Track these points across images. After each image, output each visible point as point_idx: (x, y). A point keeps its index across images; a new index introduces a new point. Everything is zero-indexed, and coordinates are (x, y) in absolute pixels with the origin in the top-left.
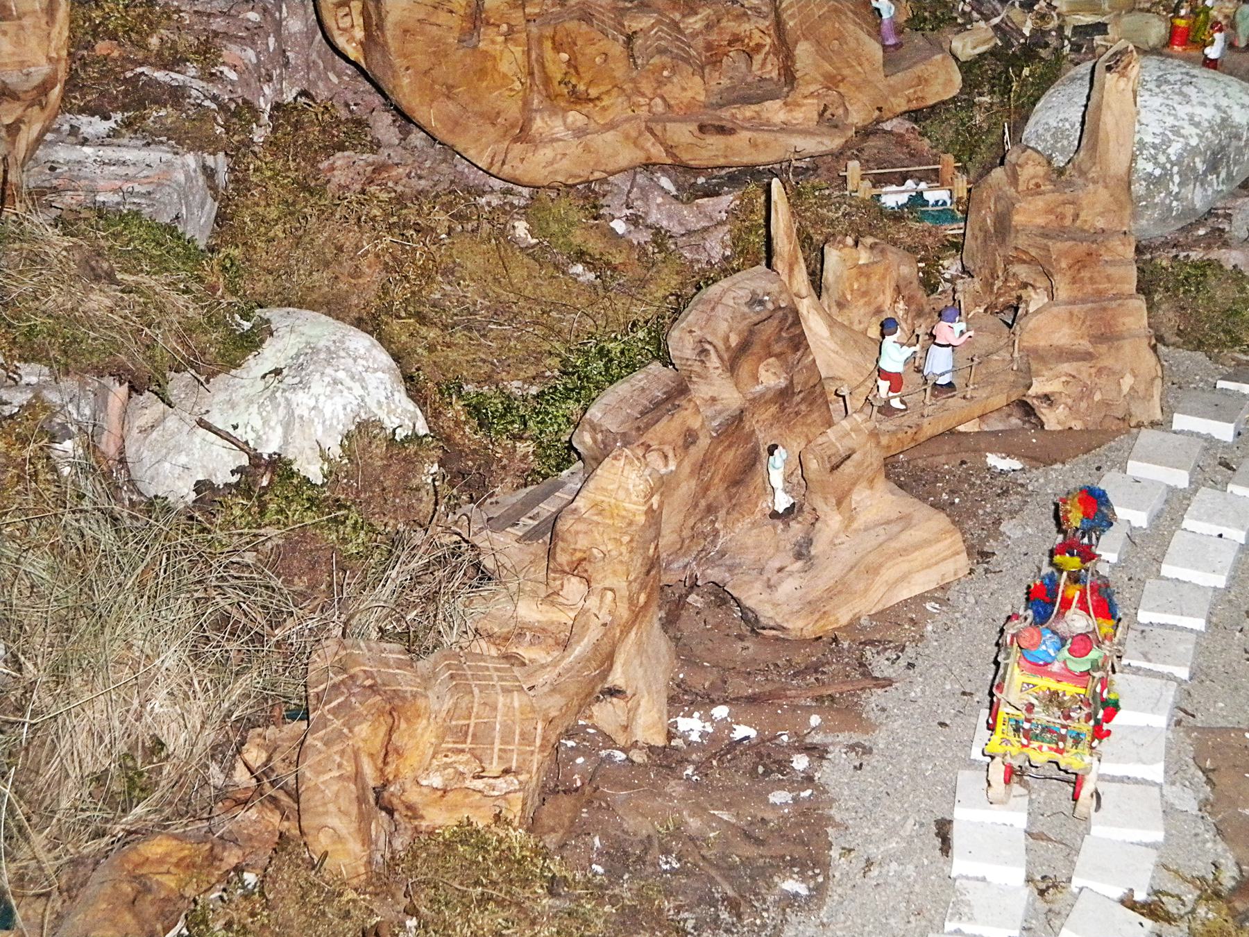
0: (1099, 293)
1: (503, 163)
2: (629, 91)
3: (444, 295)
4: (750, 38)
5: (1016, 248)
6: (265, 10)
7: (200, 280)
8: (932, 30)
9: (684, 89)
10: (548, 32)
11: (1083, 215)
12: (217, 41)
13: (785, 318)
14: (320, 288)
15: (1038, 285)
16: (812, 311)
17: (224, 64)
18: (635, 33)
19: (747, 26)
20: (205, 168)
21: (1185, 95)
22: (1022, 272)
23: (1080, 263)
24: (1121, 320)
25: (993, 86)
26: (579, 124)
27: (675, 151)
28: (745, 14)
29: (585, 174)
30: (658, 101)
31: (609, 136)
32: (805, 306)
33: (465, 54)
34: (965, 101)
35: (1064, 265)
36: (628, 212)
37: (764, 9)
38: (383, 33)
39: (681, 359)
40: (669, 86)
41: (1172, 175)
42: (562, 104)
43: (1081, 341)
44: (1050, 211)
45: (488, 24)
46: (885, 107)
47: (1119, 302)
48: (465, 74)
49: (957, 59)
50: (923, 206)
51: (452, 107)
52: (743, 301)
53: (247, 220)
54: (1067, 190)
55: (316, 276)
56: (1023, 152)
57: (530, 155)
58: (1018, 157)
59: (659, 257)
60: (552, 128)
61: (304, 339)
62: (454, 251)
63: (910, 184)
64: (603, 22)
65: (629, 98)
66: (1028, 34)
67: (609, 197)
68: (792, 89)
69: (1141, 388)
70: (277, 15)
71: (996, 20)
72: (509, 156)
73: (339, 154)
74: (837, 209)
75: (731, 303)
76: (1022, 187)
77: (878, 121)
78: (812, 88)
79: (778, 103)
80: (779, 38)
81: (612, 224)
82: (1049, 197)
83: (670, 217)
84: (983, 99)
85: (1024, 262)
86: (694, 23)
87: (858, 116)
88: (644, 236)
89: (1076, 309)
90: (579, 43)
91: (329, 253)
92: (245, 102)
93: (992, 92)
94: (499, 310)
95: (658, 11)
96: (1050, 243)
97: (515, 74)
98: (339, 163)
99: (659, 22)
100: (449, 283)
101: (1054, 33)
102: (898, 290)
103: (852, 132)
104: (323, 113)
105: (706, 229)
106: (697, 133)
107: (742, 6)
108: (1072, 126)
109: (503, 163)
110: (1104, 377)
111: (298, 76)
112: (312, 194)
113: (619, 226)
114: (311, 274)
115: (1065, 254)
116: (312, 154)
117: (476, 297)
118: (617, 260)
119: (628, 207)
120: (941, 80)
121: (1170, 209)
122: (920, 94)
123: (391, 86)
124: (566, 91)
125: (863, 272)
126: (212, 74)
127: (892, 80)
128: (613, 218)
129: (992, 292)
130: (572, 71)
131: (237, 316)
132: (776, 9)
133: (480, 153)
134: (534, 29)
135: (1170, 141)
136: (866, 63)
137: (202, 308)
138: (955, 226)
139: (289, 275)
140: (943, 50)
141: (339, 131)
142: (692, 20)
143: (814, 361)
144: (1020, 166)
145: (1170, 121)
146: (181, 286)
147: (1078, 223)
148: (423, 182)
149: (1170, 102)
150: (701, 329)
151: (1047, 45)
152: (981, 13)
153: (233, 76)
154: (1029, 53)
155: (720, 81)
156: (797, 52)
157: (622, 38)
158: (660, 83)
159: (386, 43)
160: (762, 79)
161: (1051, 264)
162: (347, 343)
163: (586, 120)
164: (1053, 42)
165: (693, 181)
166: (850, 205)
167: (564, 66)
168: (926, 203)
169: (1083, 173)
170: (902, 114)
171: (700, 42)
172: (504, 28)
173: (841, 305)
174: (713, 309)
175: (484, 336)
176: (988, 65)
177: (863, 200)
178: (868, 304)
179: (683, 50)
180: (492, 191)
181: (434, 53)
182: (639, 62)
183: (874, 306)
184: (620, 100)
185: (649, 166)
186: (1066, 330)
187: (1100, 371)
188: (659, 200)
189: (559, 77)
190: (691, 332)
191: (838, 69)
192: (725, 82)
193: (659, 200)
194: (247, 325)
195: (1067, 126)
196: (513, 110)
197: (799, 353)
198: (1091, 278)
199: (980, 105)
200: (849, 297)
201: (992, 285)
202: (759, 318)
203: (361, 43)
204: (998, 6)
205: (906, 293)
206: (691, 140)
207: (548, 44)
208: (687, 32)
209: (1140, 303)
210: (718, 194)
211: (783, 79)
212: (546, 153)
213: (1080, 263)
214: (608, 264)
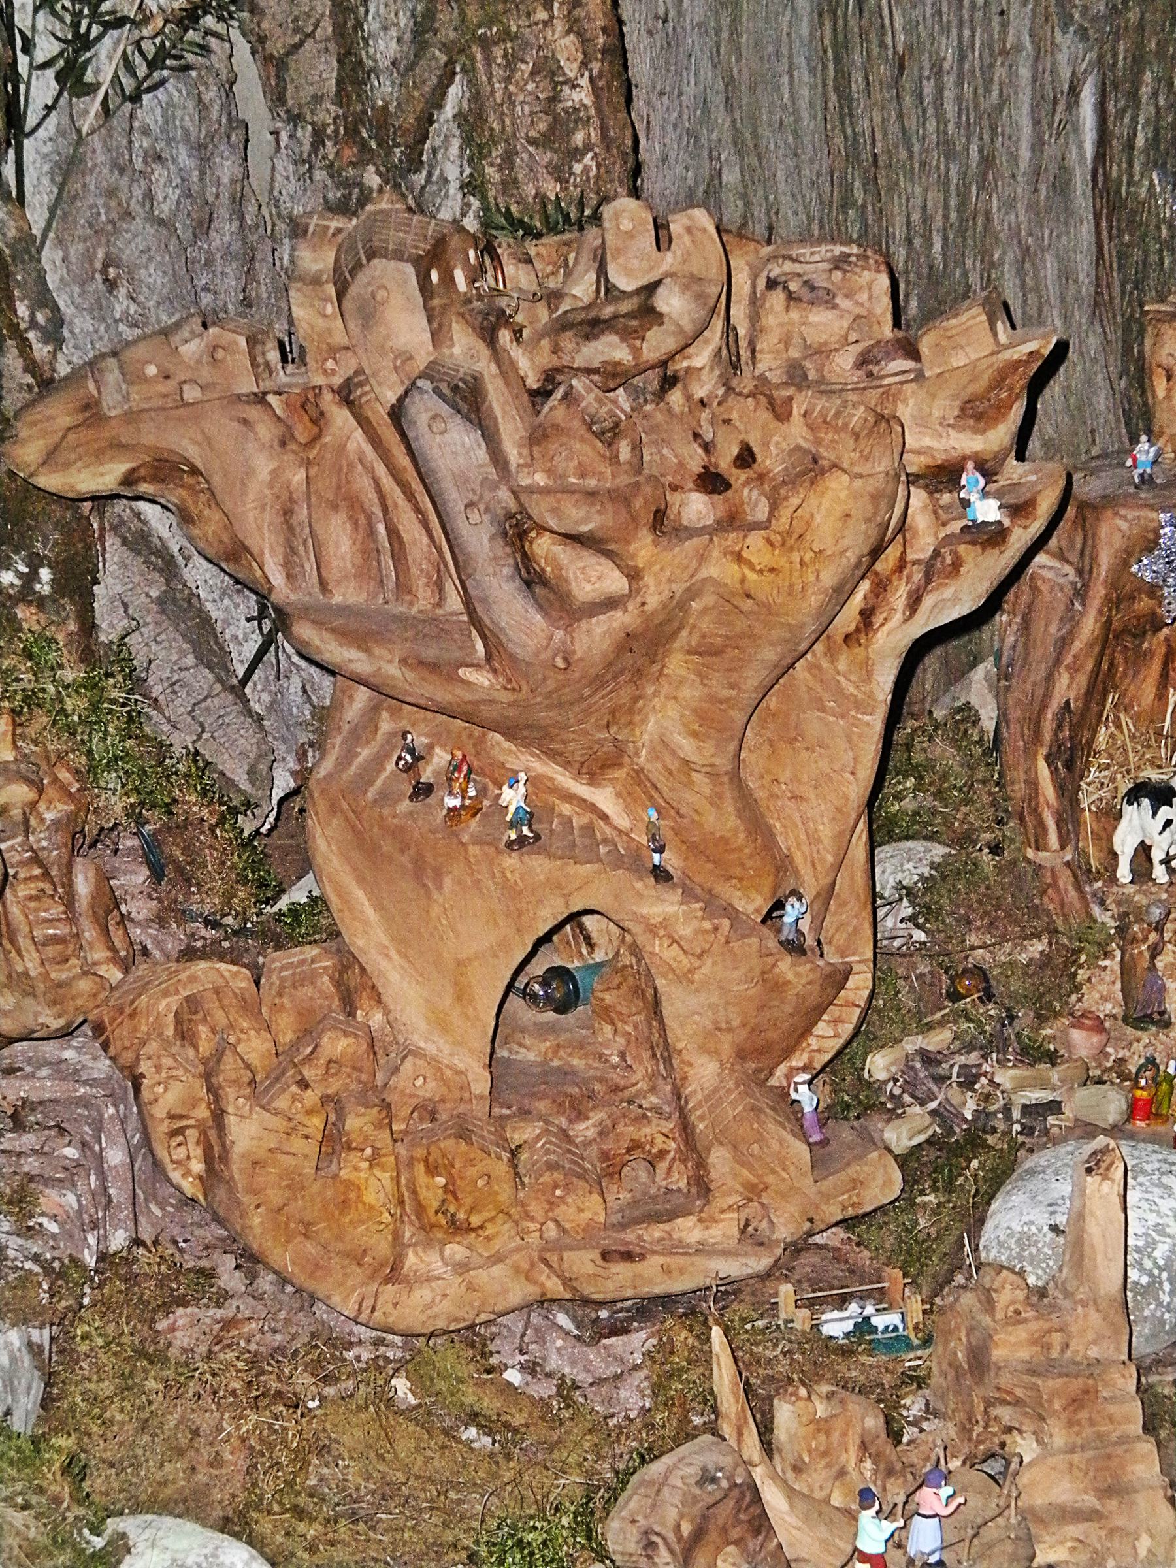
0: (1100, 1436)
1: (373, 1310)
2: (517, 1217)
3: (321, 1480)
4: (652, 1143)
5: (998, 1389)
6: (84, 1144)
7: (41, 1490)
8: (858, 1117)
9: (580, 1210)
10: (420, 1152)
11: (1073, 1344)
12: (33, 1185)
13: (743, 1494)
14: (174, 1482)
15: (1024, 1428)
16: (768, 1482)
17: (42, 1214)
18: (520, 1146)
19: (648, 1130)
20: (30, 1344)
21: (1166, 1187)
22: (1005, 1414)
23: (1076, 1403)
24: (1129, 1469)
25: (935, 1181)
26: (458, 1257)
27: (574, 1284)
28: (644, 1116)
29: (470, 1317)
30: (551, 1225)
31: (497, 1270)
32: (758, 1474)
33: (324, 1186)
34: (906, 1201)
35: (1057, 1406)
36: (522, 1358)
37: (667, 1109)
38: (228, 1168)
39: (622, 1554)
40: (563, 1207)
41: (1161, 1283)
42: (439, 1236)
43: (1085, 1497)
44: (1035, 1342)
45: (350, 1148)
46: (816, 1218)
47: (1125, 1447)
48: (325, 1207)
49: (890, 1151)
50: (870, 1333)
51: (310, 1248)
52: (693, 1481)
53: (78, 1400)
54: (1054, 1316)
55: (168, 1467)
56: (999, 1273)
57: (404, 1298)
58: (993, 1281)
59: (566, 1414)
60: (429, 1264)
61: (168, 1556)
62: (328, 1426)
63: (853, 1308)
64: (483, 1137)
65: (517, 1223)
66: (969, 1117)
67: (498, 1341)
68: (708, 1202)
69: (1160, 1552)
70: (97, 1148)
71: (933, 1105)
72: (379, 1303)
73: (180, 1311)
74: (775, 1345)
75: (679, 1483)
76: (999, 1315)
77: (810, 1234)
78: (732, 1200)
79: (691, 1220)
80: (687, 1143)
81: (506, 1375)
82: (1034, 1326)
83: (573, 1363)
84: (926, 1199)
85: (1009, 1403)
86: (585, 1130)
87: (785, 1230)
88: (544, 1389)
89: (1076, 1458)
90: (457, 1166)
91: (183, 1439)
92: (73, 1259)
93: (935, 1189)
94: (387, 1493)
95: (540, 1118)
96: (1040, 1382)
97: (384, 1205)
98: (180, 1322)
99: (546, 1132)
100: (327, 1465)
101: (1000, 1116)
102: (864, 1446)
103: (779, 1251)
104: (159, 1264)
105: (618, 1377)
106: (599, 1261)
107: (640, 1107)
108: (1040, 1231)
109: (373, 1310)
110: (1116, 1540)
111: (122, 1216)
112: (151, 1363)
113: (514, 1376)
114: (162, 1465)
115: (1054, 1394)
116: (150, 1312)
117: (360, 1480)
118: (518, 1420)
119: (522, 1353)
120: (879, 1181)
121: (1162, 1322)
122: (855, 1199)
123: (238, 1228)
124: (444, 1222)
125: (821, 1426)
126: (29, 1228)
127: (826, 1185)
128: (506, 1367)
129: (970, 1440)
130: (450, 1197)
131: (86, 1532)
132: (682, 1110)
133: (345, 1299)
134: (402, 1150)
135: (1155, 1242)
136: (792, 1168)
137: (45, 1525)
138: (911, 1355)
139: (137, 1467)
140: (877, 1148)
141: (179, 1283)
142: (582, 1126)
143: (780, 1546)
144: (996, 1291)
145: (1153, 1219)
146: (19, 1500)
147: (1069, 1353)
148: (278, 1337)
149: (1149, 1196)
150: (646, 1517)
151: (994, 1130)
152: (913, 1096)
153: (54, 1228)
154: (974, 1141)
155: (619, 1195)
156: (710, 1161)
157: (506, 1156)
158: (552, 1205)
159: (232, 1177)
160: (669, 1191)
161: (1042, 1405)
162: (221, 1558)
163: (468, 1253)
164: (999, 1123)
165: (593, 1315)
166: (790, 1341)
167: (440, 1191)
168: (874, 1330)
169: (1067, 1295)
170: (837, 1224)
171: (593, 1151)
172: (368, 1151)
173: (798, 1469)
174: (659, 1491)
175: (373, 1528)
176: (931, 1154)
177: (803, 1332)
178: (828, 1466)
179: (575, 1163)
180: (360, 1342)
181: (288, 1186)
182: (526, 1180)
183: (837, 1467)
184: (507, 1226)
185: (545, 1302)
186: (1066, 1484)
187: (1111, 1532)
188: (559, 1343)
189: (435, 1204)
190: (634, 1521)
191: (758, 1176)
192: (625, 1196)
193: (559, 1343)
194: (98, 1542)
195: (1034, 1229)
196: (382, 1246)
197: (760, 1538)
198: (1090, 1419)
199: (924, 1206)
200: (807, 1460)
201: (971, 1431)
202: (711, 1500)
203: (200, 1177)
204: (935, 1089)
205: (873, 1450)
206: (590, 1269)
207: (420, 1168)
208: (578, 1140)
209: (1148, 1447)
210: (626, 1331)
211: (694, 1190)
212: (422, 1294)
213: (1076, 1403)
214: (507, 1426)
